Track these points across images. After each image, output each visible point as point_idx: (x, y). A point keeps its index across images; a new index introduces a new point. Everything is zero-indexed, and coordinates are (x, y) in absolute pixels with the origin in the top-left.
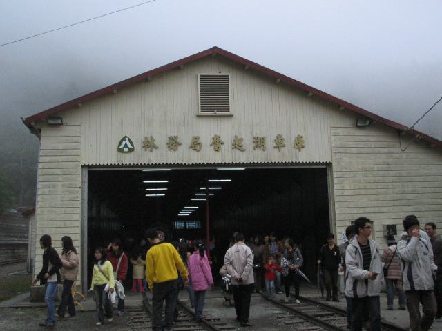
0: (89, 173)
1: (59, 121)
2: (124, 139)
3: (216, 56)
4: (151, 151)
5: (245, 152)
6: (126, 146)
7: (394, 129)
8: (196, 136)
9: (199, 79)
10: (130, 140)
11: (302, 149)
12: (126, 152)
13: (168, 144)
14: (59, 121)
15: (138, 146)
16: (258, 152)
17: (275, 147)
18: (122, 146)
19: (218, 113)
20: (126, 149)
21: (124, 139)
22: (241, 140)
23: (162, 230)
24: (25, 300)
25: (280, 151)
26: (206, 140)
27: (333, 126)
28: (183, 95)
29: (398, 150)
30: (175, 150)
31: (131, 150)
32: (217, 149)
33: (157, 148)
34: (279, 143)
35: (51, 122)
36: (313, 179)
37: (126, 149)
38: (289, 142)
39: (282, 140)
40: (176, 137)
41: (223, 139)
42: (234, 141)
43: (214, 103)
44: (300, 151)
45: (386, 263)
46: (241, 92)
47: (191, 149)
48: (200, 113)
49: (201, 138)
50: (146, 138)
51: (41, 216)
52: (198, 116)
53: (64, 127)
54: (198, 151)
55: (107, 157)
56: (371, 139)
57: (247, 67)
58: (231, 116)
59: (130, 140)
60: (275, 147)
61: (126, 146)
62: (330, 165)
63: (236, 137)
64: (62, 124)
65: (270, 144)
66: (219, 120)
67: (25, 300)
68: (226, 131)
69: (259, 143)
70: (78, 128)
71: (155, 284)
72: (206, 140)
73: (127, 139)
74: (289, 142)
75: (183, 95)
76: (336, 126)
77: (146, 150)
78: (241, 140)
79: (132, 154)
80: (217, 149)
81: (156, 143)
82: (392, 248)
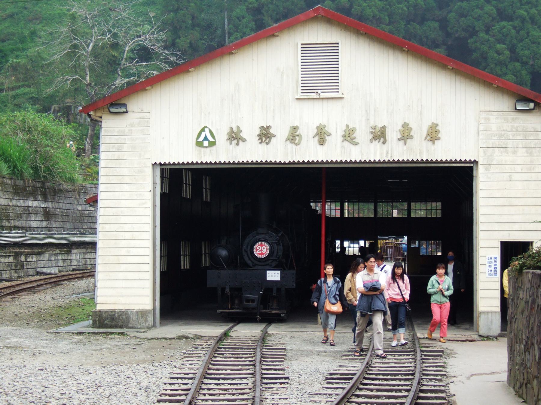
0: (162, 171)
1: (124, 110)
2: (203, 130)
4: (238, 144)
5: (357, 146)
6: (206, 138)
8: (295, 125)
10: (211, 132)
11: (436, 142)
12: (206, 147)
13: (259, 135)
15: (222, 138)
16: (377, 145)
17: (399, 139)
18: (201, 139)
19: (323, 95)
20: (206, 143)
21: (203, 130)
22: (353, 130)
23: (266, 241)
24: (87, 327)
25: (405, 144)
26: (308, 132)
27: (483, 109)
29: (121, 340)
30: (267, 144)
31: (212, 144)
32: (322, 142)
33: (244, 140)
34: (406, 135)
35: (112, 110)
36: (453, 184)
37: (206, 143)
38: (419, 132)
39: (409, 129)
40: (268, 127)
41: (328, 129)
42: (345, 131)
44: (434, 143)
45: (537, 253)
47: (288, 142)
48: (300, 96)
49: (301, 127)
50: (231, 128)
54: (297, 145)
55: (186, 154)
59: (211, 132)
60: (399, 139)
61: (206, 138)
62: (476, 162)
63: (347, 126)
64: (127, 112)
65: (392, 135)
66: (325, 102)
67: (88, 327)
68: (331, 116)
69: (379, 135)
71: (286, 289)
72: (308, 132)
73: (207, 130)
74: (419, 132)
76: (488, 109)
77: (231, 144)
78: (353, 130)
79: (214, 148)
80: (322, 142)
81: (243, 135)
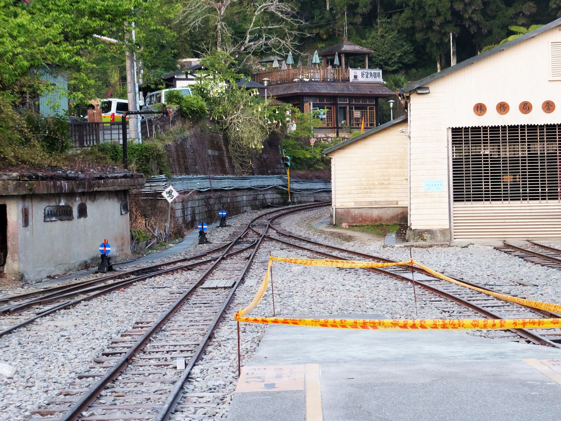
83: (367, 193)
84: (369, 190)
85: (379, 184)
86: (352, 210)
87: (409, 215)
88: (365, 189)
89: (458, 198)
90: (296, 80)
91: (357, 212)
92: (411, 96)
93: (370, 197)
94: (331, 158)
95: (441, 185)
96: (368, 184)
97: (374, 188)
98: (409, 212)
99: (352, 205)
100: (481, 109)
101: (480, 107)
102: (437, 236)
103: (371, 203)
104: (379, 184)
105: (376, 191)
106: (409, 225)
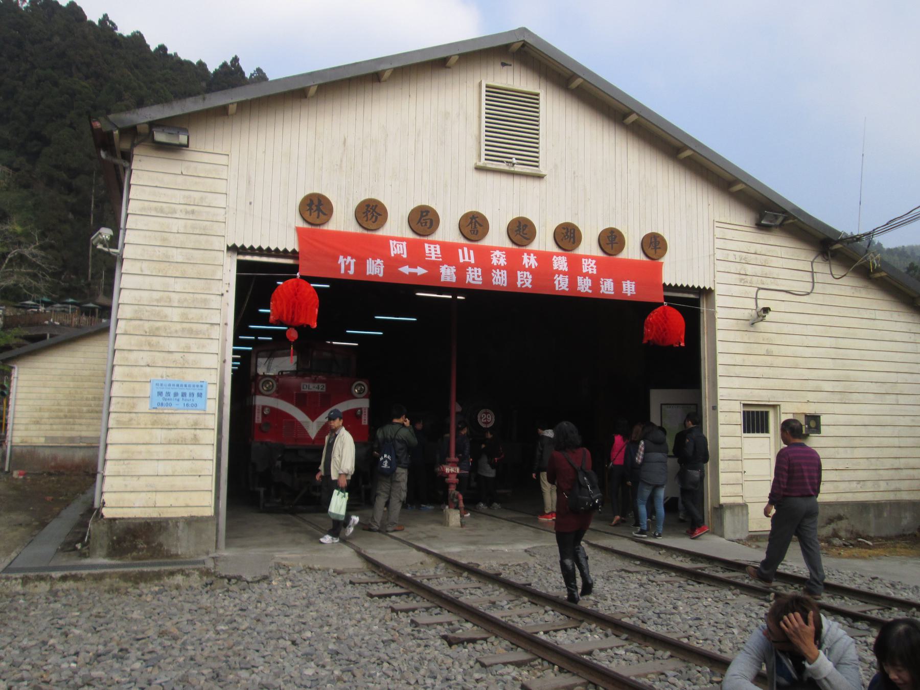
3: (522, 52)
7: (719, 177)
9: (484, 93)
14: (183, 139)
19: (518, 168)
28: (456, 109)
35: (160, 137)
43: (510, 143)
46: (557, 117)
48: (483, 162)
51: (126, 354)
52: (479, 169)
53: (188, 155)
56: (785, 259)
57: (574, 85)
58: (540, 177)
62: (707, 293)
70: (223, 160)
75: (456, 109)
82: (773, 424)
83: (68, 424)
84: (71, 420)
85: (88, 412)
86: (40, 451)
87: (99, 477)
88: (66, 417)
89: (744, 432)
90: (47, 322)
91: (47, 452)
92: (136, 151)
93: (72, 430)
94: (13, 368)
95: (200, 395)
96: (70, 411)
97: (80, 418)
98: (100, 469)
99: (41, 441)
100: (319, 210)
101: (316, 202)
102: (178, 539)
103: (72, 439)
104: (88, 412)
105: (84, 421)
106: (96, 505)
